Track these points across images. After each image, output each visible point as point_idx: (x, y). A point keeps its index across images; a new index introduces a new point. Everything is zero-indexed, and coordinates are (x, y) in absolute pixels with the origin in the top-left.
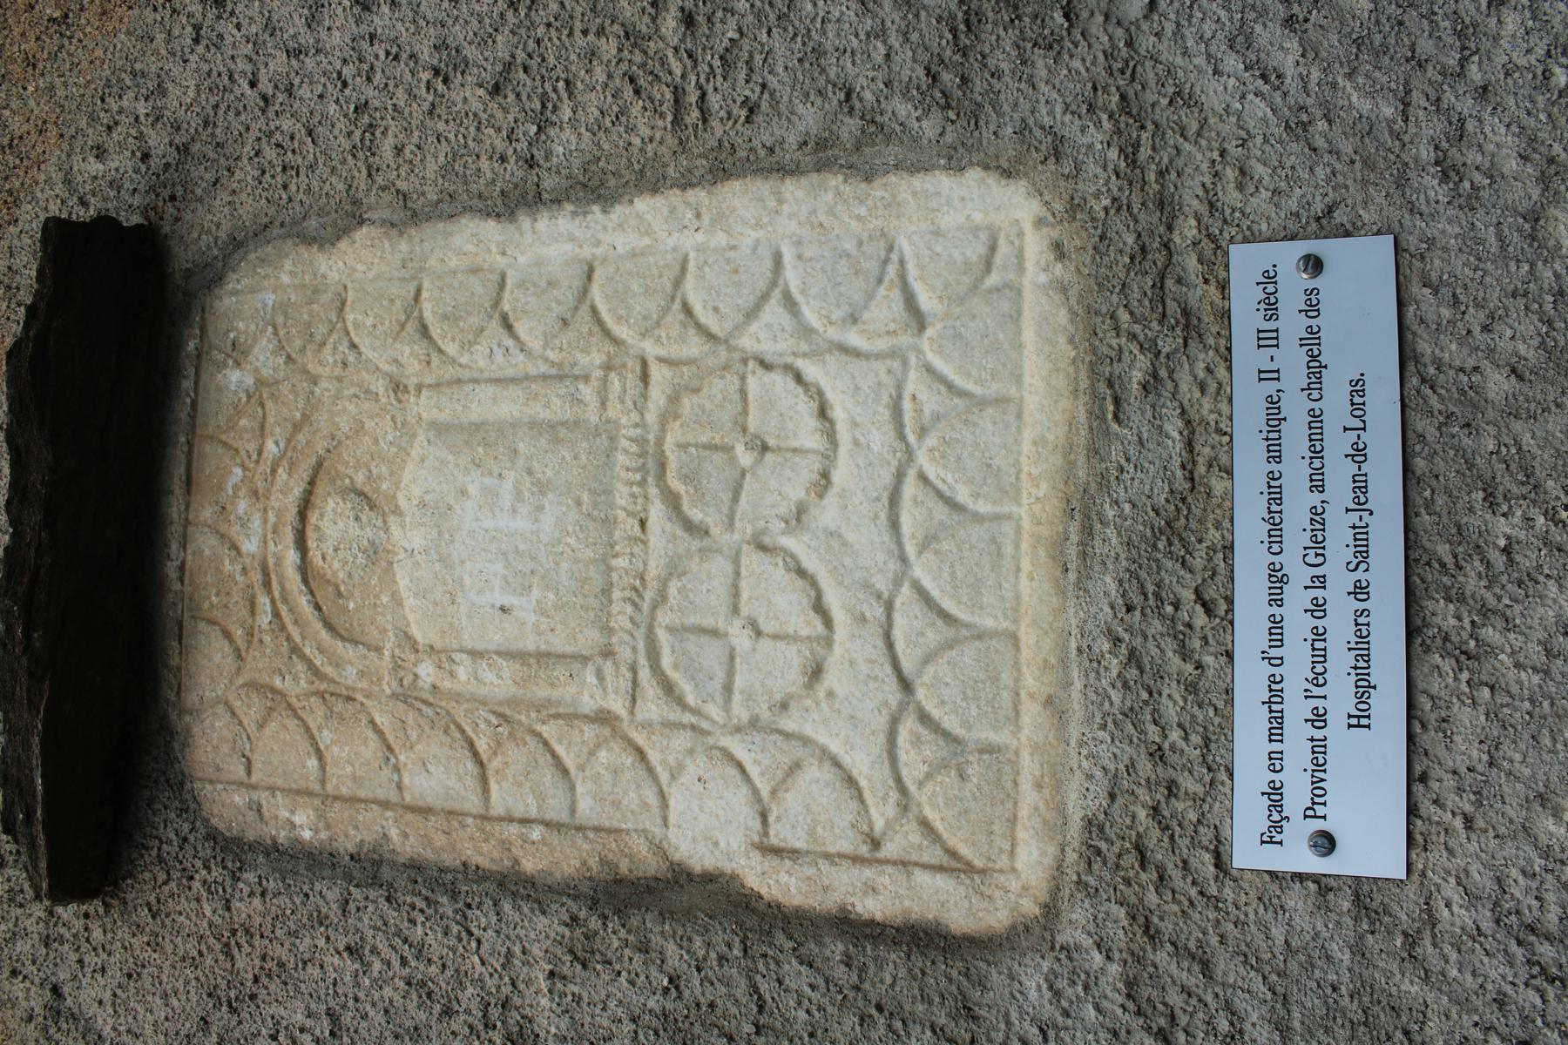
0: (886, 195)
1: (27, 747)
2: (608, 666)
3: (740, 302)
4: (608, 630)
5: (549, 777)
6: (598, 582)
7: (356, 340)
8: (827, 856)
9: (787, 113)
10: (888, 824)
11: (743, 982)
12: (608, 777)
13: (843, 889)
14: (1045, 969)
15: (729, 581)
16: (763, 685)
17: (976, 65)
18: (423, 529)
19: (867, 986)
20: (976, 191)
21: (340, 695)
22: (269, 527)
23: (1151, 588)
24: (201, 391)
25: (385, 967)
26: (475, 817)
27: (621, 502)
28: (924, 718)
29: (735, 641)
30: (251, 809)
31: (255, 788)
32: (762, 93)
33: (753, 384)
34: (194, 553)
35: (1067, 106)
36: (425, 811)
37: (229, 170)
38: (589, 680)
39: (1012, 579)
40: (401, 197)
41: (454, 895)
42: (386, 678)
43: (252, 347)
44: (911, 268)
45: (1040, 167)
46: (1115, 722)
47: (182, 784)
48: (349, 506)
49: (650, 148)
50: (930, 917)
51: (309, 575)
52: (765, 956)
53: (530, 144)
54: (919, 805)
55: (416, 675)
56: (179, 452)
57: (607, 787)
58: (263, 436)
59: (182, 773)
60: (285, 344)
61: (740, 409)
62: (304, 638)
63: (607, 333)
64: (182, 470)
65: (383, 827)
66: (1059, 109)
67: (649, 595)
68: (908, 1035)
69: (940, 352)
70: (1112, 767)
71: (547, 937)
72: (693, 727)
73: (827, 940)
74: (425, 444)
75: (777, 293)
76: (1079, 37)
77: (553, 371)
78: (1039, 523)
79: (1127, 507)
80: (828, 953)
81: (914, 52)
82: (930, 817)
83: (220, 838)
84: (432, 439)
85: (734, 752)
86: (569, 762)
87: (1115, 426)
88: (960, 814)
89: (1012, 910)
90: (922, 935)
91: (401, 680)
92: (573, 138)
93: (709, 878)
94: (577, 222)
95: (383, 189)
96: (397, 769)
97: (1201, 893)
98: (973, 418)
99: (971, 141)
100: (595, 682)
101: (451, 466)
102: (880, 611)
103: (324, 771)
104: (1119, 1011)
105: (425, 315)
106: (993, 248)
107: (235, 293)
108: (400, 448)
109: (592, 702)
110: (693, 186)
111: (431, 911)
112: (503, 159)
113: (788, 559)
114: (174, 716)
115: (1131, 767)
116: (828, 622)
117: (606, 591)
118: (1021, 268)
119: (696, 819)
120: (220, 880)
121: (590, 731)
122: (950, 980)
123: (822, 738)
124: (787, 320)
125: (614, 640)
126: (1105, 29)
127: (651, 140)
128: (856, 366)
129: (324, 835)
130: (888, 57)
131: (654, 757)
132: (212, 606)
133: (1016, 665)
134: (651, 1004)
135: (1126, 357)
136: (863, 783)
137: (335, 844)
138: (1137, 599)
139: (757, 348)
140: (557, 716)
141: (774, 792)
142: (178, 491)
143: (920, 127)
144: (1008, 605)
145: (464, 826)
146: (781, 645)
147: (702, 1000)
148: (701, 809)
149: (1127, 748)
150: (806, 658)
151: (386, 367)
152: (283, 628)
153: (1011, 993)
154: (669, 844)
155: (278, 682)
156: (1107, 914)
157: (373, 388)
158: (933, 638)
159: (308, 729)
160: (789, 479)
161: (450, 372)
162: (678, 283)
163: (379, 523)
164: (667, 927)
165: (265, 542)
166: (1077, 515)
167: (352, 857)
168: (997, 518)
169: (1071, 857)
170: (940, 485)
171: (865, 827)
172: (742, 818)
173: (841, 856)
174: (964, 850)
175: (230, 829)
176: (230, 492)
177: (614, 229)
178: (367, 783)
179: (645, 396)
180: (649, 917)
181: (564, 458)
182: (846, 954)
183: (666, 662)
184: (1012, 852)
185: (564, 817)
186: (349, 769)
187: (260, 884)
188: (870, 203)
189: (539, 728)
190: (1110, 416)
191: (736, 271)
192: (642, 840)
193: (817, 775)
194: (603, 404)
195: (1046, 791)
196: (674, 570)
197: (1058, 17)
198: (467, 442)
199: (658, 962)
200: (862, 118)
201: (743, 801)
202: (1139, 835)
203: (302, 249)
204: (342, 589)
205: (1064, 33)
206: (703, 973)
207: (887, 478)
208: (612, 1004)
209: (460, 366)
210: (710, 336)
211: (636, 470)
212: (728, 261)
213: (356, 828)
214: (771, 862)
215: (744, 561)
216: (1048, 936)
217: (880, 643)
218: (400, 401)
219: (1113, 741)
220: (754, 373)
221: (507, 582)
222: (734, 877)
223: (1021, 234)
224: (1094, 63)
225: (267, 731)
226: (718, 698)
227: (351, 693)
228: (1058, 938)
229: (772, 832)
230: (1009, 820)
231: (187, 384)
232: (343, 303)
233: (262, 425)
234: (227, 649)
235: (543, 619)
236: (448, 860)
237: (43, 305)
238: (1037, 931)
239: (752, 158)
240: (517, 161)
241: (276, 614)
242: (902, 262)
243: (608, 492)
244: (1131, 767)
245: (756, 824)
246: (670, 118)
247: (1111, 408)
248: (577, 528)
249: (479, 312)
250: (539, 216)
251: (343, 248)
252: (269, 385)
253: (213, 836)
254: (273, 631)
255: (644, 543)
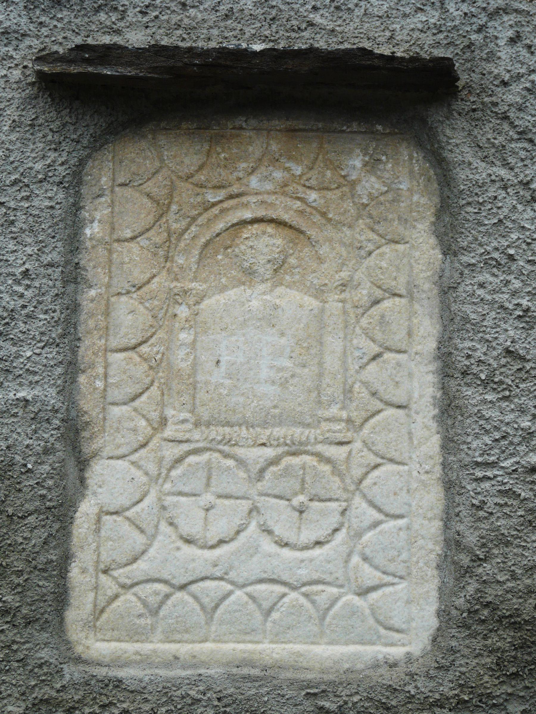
1: (130, 64)
3: (378, 497)
4: (208, 424)
5: (130, 391)
6: (234, 419)
7: (373, 255)
9: (476, 525)
10: (115, 578)
11: (32, 508)
12: (132, 425)
14: (51, 661)
15: (233, 494)
16: (181, 513)
18: (262, 308)
19: (37, 573)
21: (168, 252)
24: (350, 136)
25: (19, 294)
26: (105, 344)
28: (167, 596)
31: (112, 191)
32: (488, 512)
33: (333, 505)
34: (250, 137)
35: (464, 674)
36: (107, 314)
38: (182, 414)
39: (234, 639)
41: (63, 336)
42: (179, 285)
43: (375, 175)
44: (391, 589)
45: (434, 658)
49: (465, 447)
50: (71, 601)
51: (237, 227)
52: (47, 518)
53: (475, 374)
54: (125, 594)
63: (366, 420)
64: (301, 127)
66: (463, 669)
67: (226, 448)
72: (159, 474)
74: (310, 308)
75: (381, 517)
76: (501, 680)
79: (266, 699)
81: (500, 596)
82: (120, 599)
84: (313, 312)
85: (147, 497)
86: (136, 403)
87: (304, 693)
88: (121, 615)
89: (77, 641)
90: (63, 597)
91: (178, 295)
92: (474, 401)
94: (431, 400)
95: (462, 274)
96: (128, 292)
99: (451, 623)
100: (181, 418)
102: (218, 574)
103: (124, 241)
105: (385, 301)
106: (398, 631)
107: (411, 158)
109: (170, 416)
110: (444, 469)
113: (244, 526)
115: (146, 700)
116: (212, 547)
117: (228, 424)
118: (386, 645)
119: (113, 475)
122: (42, 614)
124: (366, 524)
125: (203, 428)
126: (503, 693)
127: (469, 448)
129: (88, 244)
130: (498, 582)
131: (143, 452)
132: (219, 154)
133: (193, 642)
135: (336, 699)
136: (135, 566)
137: (84, 251)
138: (225, 701)
141: (128, 519)
143: (461, 597)
144: (222, 637)
152: (206, 210)
153: (39, 644)
154: (99, 460)
155: (174, 207)
156: (79, 689)
157: (345, 268)
159: (148, 230)
160: (285, 526)
162: (391, 460)
165: (256, 194)
166: (262, 674)
167: (77, 264)
170: (280, 604)
171: (113, 567)
172: (114, 501)
174: (105, 616)
176: (287, 165)
178: (119, 272)
179: (331, 443)
181: (300, 397)
182: (52, 561)
183: (192, 459)
184: (104, 640)
185: (109, 399)
186: (127, 260)
189: (156, 384)
190: (309, 691)
191: (395, 494)
193: (138, 543)
194: (328, 420)
196: (241, 462)
197: (513, 670)
199: (39, 461)
200: (468, 567)
201: (123, 502)
205: (504, 672)
206: (36, 486)
207: (285, 577)
208: (15, 436)
209: (354, 327)
212: (401, 489)
213: (94, 267)
215: (244, 502)
217: (203, 575)
219: (158, 691)
220: (340, 506)
221: (233, 364)
223: (403, 645)
224: (486, 688)
225: (145, 200)
226: (174, 489)
229: (108, 517)
230: (119, 638)
232: (397, 242)
235: (213, 387)
236: (81, 329)
239: (455, 504)
240: (466, 365)
241: (214, 205)
242: (393, 584)
244: (146, 700)
246: (479, 460)
248: (262, 407)
249: (384, 339)
250: (435, 376)
254: (204, 204)
255: (253, 446)
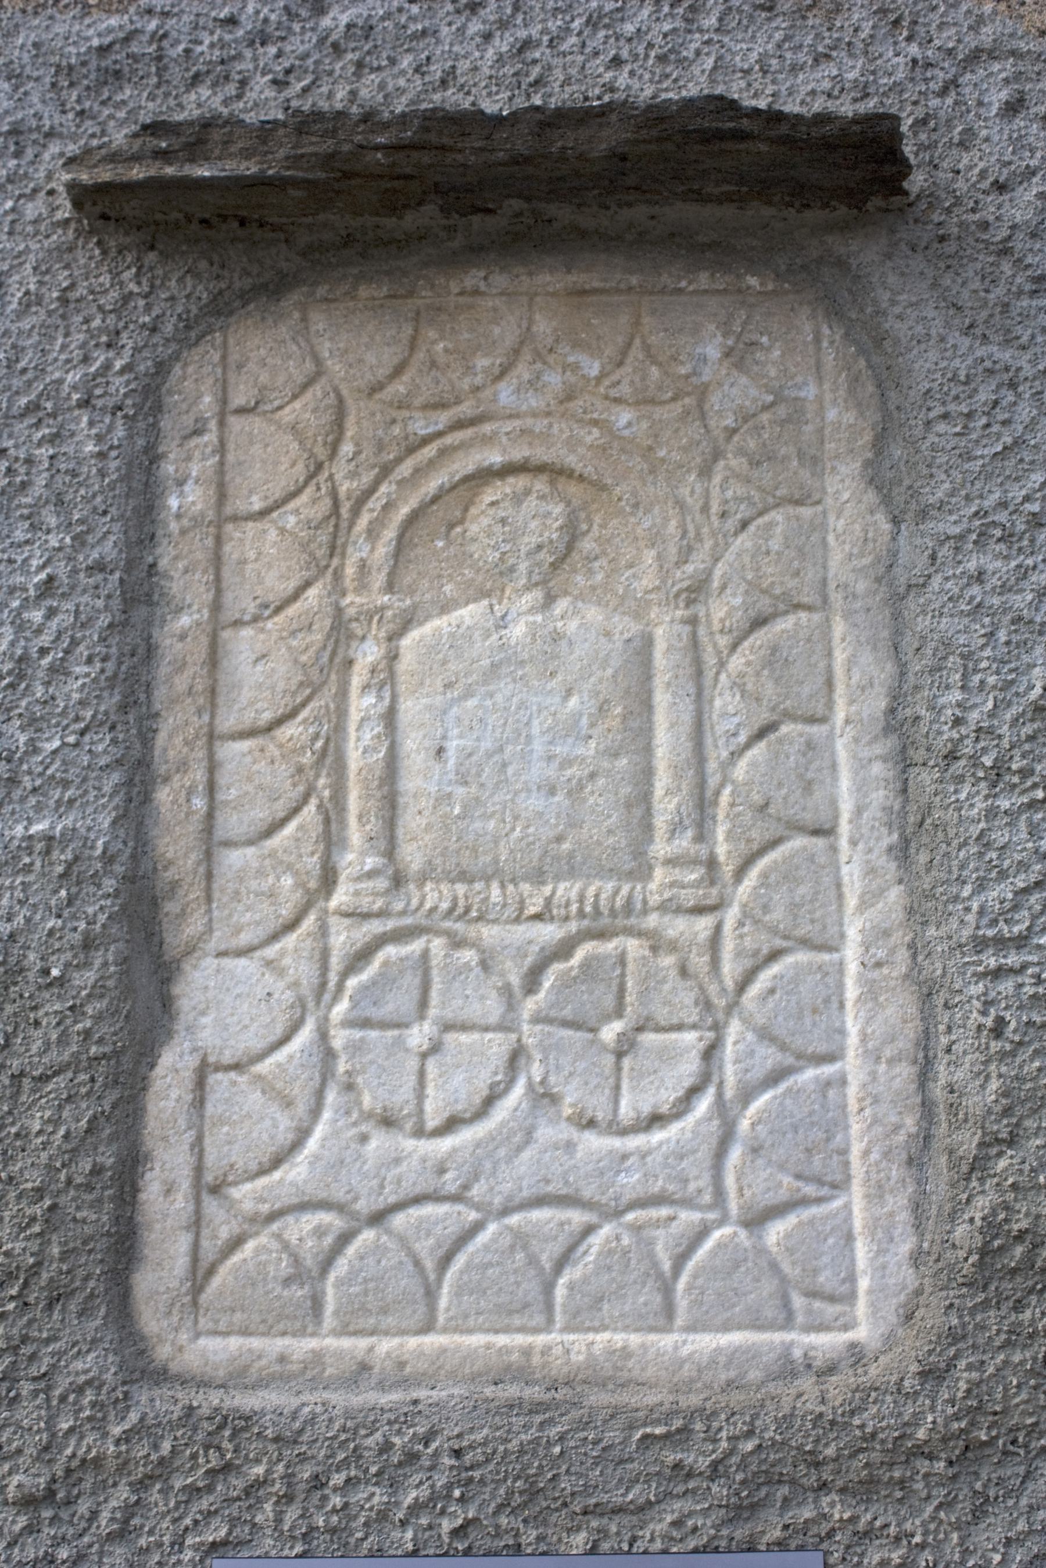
0: (892, 1182)
2: (382, 883)
4: (422, 879)
7: (752, 528)
8: (199, 1139)
13: (166, 1157)
17: (1030, 1283)
20: (893, 1281)
22: (529, 421)
23: (477, 1474)
26: (211, 724)
27: (562, 886)
28: (345, 1239)
29: (415, 1030)
30: (196, 421)
33: (690, 1037)
36: (213, 660)
37: (971, 326)
40: (921, 581)
41: (123, 708)
44: (814, 1210)
46: (347, 1440)
47: (219, 313)
48: (554, 536)
52: (93, 1080)
55: (364, 638)
56: (618, 276)
57: (254, 884)
58: (637, 403)
59: (231, 313)
60: (750, 423)
61: (663, 1023)
62: (399, 483)
64: (596, 284)
65: (190, 606)
68: (27, 1239)
69: (720, 1246)
70: (305, 1438)
71: (89, 829)
72: (323, 985)
73: (114, 1147)
74: (626, 636)
77: (709, 794)
78: (543, 1353)
80: (101, 1149)
83: (159, 380)
87: (638, 1435)
89: (158, 1336)
91: (357, 620)
93: (167, 1004)
94: (879, 814)
96: (256, 619)
97: (187, 1529)
98: (650, 1283)
100: (367, 868)
101: (599, 673)
102: (452, 1188)
104: (69, 1451)
106: (832, 1299)
108: (623, 598)
111: (103, 684)
112: (958, 722)
114: (295, 296)
117: (464, 877)
118: (808, 1329)
120: (112, 389)
121: (312, 863)
123: (319, 1131)
124: (757, 1074)
128: (705, 1153)
129: (174, 526)
131: (290, 940)
134: (32, 956)
136: (277, 1175)
137: (165, 541)
138: (468, 1458)
139: (730, 1040)
140: (327, 821)
141: (259, 1077)
142: (572, 278)
145: (199, 712)
146: (412, 1080)
147: (41, 1013)
148: (238, 996)
149: (323, 1452)
150: (401, 1109)
151: (718, 573)
152: (411, 450)
158: (424, 1247)
161: (710, 660)
162: (806, 943)
163: (536, 578)
164: (112, 969)
165: (511, 417)
168: (549, 1307)
169: (215, 1398)
170: (581, 1249)
173: (201, 1152)
174: (216, 1282)
175: (170, 393)
176: (571, 359)
177: (868, 862)
179: (679, 910)
180: (121, 945)
181: (609, 816)
183: (391, 951)
185: (219, 834)
186: (252, 555)
187: (111, 448)
188: (884, 1164)
189: (313, 802)
190: (648, 1430)
191: (815, 1011)
192: (200, 928)
195: (277, 1368)
198: (627, 692)
202: (239, 1467)
203: (868, 437)
204: (459, 529)
207: (587, 1193)
209: (718, 673)
210: (742, 987)
211: (596, 905)
214: (188, 1075)
215: (499, 1036)
216: (137, 1375)
217: (418, 1190)
218: (677, 596)
221: (470, 755)
222: (170, 1034)
227: (338, 550)
228: (136, 1387)
229: (220, 1076)
231: (704, 280)
233: (652, 401)
234: (382, 373)
236: (160, 693)
237: (784, 129)
238: (140, 1364)
242: (819, 1200)
243: (572, 873)
245: (227, 1058)
247: (658, 1431)
250: (890, 765)
251: (865, 498)
252: (700, 406)
253: (162, 369)
255: (517, 920)
